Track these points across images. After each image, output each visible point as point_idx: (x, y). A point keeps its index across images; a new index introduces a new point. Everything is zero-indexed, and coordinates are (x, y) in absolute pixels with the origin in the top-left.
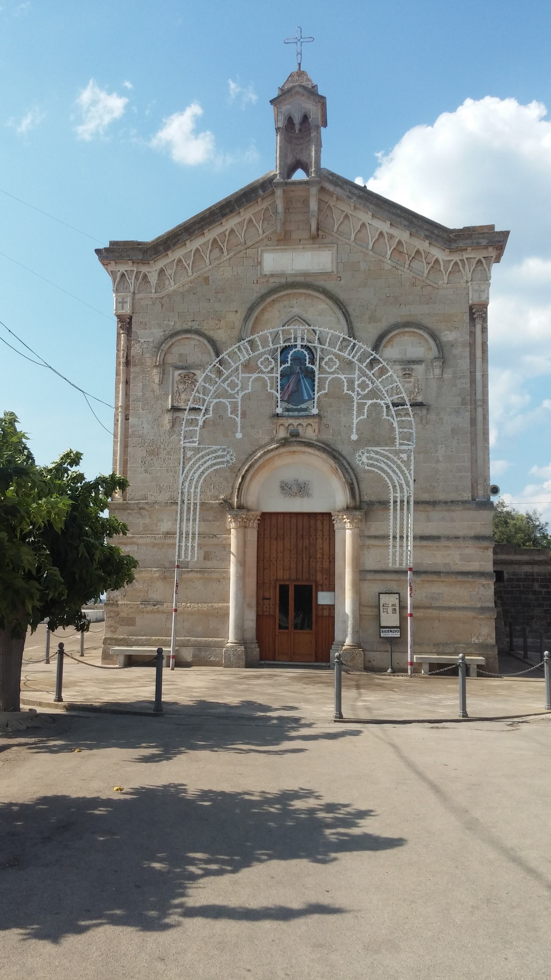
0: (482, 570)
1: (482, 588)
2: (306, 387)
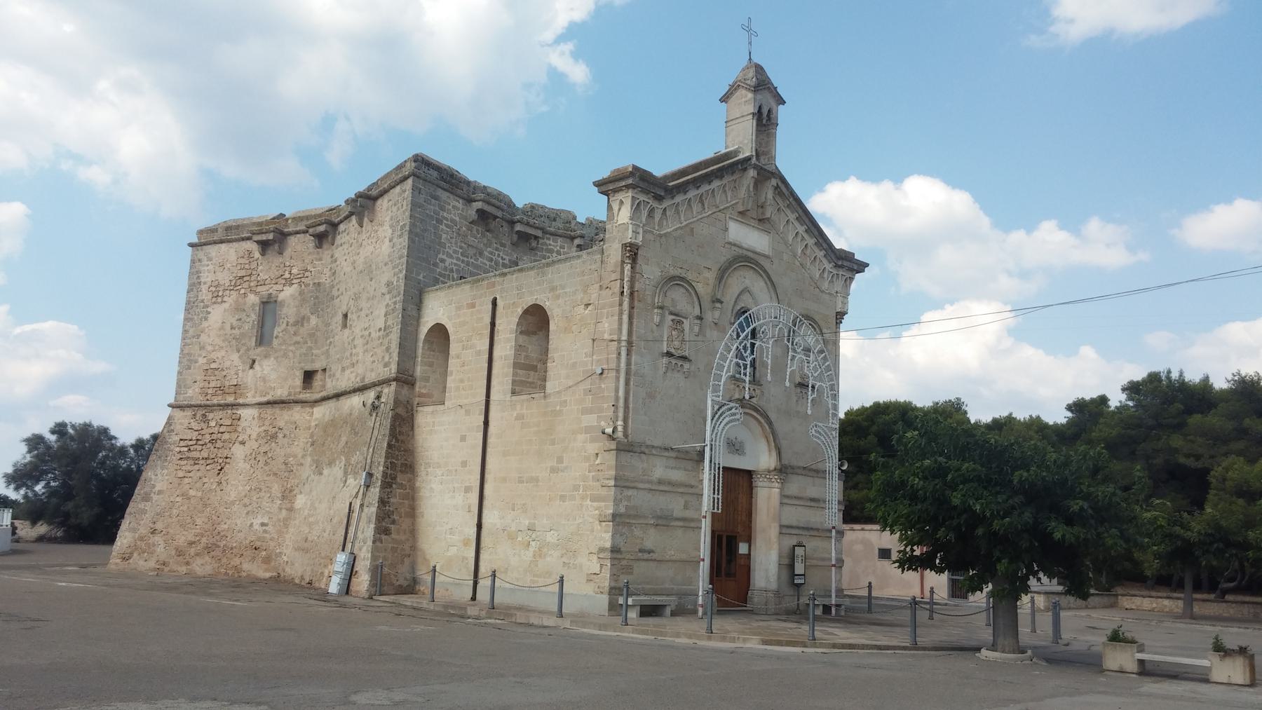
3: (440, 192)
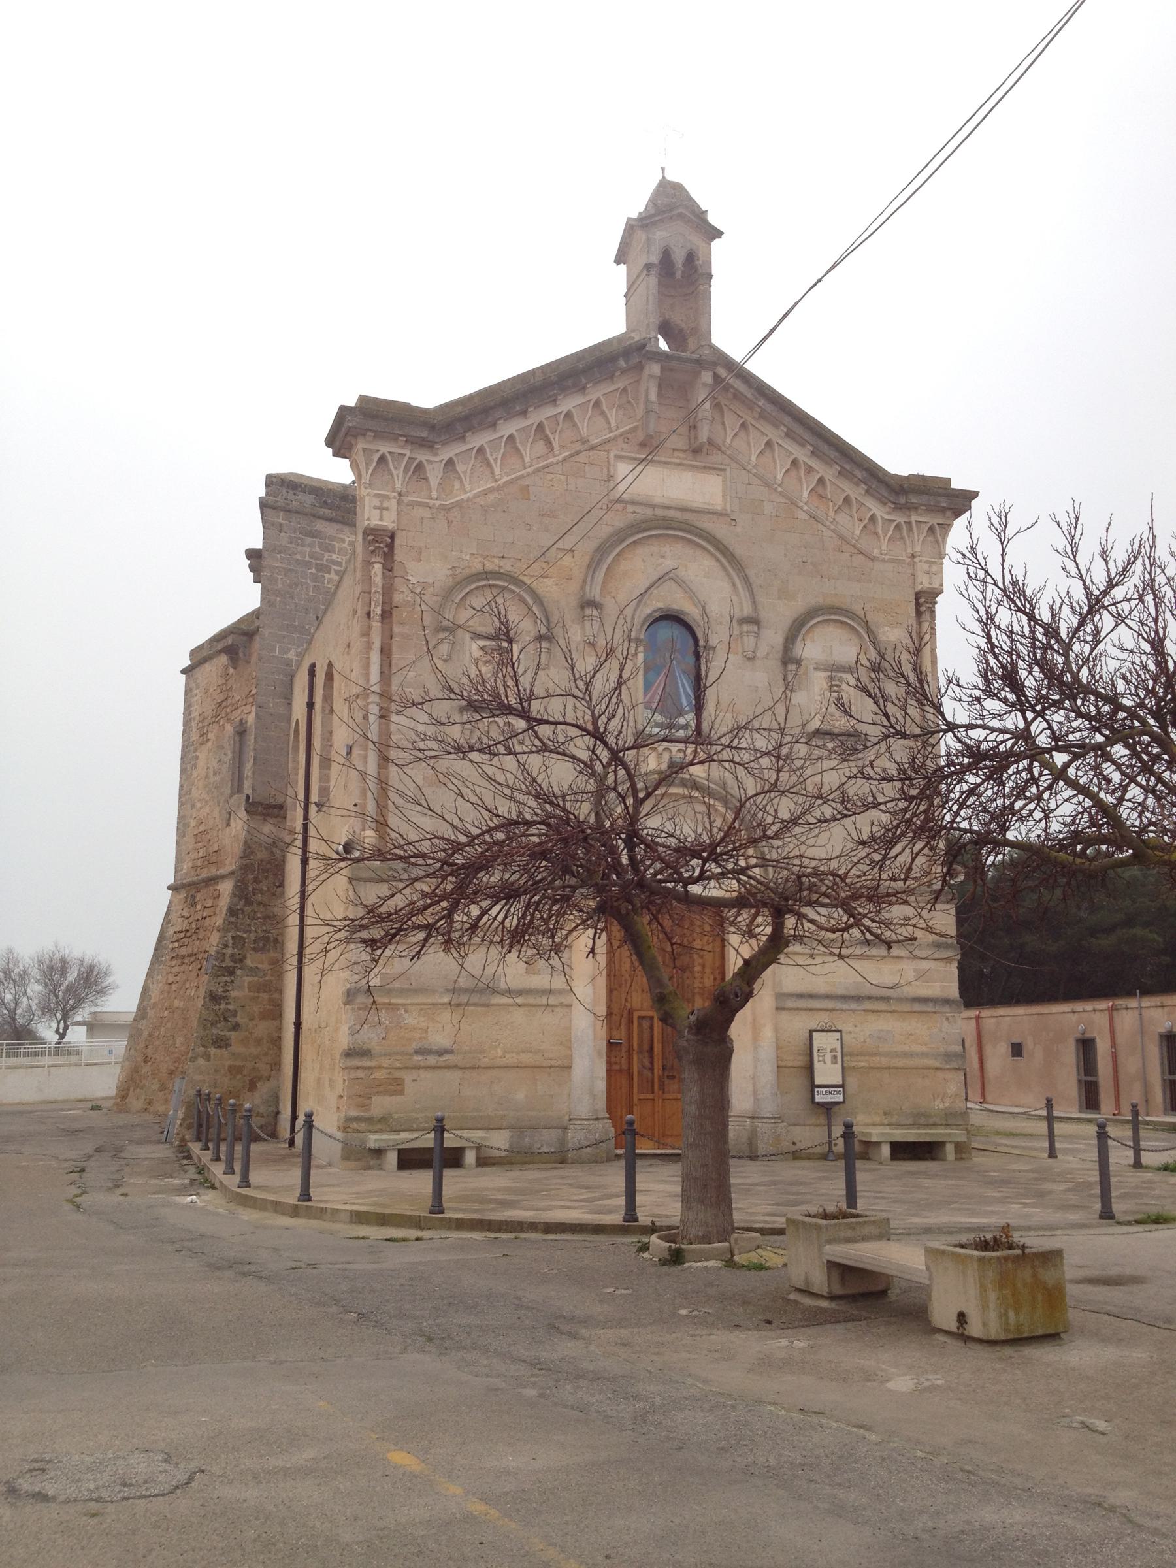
0: (945, 995)
1: (946, 1023)
2: (684, 688)
3: (320, 525)
